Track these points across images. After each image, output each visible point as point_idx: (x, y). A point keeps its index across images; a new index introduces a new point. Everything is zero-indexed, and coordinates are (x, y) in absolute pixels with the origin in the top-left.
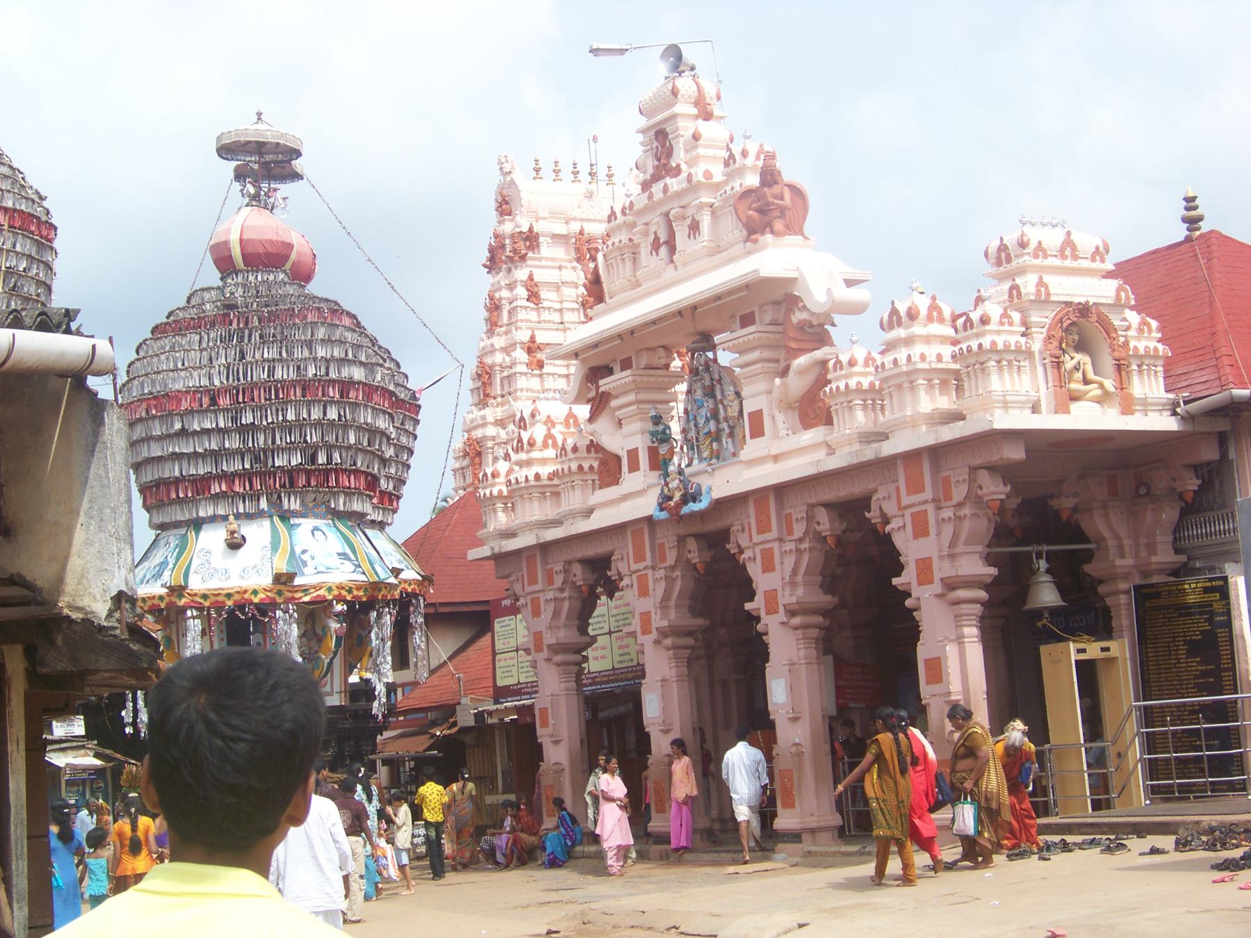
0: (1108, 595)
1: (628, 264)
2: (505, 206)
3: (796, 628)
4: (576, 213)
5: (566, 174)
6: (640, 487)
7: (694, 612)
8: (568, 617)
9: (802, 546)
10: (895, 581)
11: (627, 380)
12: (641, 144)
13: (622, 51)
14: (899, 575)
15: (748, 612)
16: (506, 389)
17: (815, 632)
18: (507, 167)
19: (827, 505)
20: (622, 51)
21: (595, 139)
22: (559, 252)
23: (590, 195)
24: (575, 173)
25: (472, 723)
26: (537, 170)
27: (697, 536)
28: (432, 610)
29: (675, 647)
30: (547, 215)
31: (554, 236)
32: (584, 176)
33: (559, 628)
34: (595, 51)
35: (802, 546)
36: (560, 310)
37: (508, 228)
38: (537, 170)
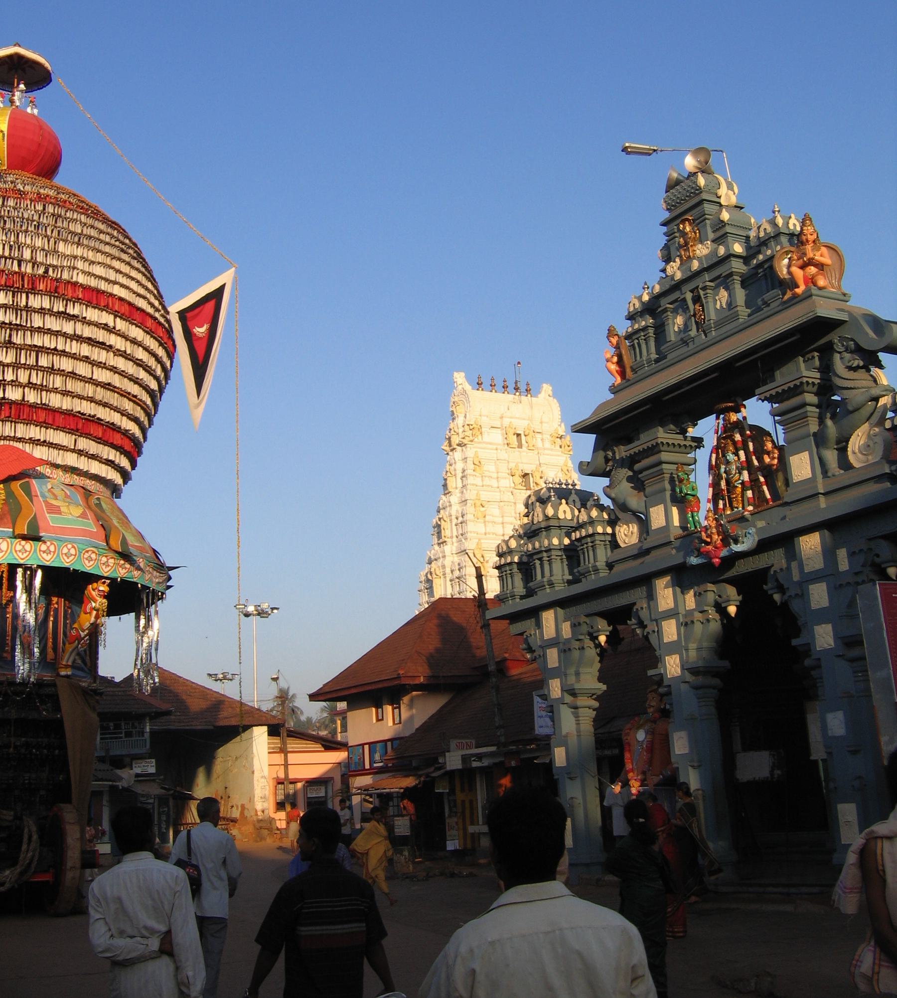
15: (794, 647)
19: (885, 537)
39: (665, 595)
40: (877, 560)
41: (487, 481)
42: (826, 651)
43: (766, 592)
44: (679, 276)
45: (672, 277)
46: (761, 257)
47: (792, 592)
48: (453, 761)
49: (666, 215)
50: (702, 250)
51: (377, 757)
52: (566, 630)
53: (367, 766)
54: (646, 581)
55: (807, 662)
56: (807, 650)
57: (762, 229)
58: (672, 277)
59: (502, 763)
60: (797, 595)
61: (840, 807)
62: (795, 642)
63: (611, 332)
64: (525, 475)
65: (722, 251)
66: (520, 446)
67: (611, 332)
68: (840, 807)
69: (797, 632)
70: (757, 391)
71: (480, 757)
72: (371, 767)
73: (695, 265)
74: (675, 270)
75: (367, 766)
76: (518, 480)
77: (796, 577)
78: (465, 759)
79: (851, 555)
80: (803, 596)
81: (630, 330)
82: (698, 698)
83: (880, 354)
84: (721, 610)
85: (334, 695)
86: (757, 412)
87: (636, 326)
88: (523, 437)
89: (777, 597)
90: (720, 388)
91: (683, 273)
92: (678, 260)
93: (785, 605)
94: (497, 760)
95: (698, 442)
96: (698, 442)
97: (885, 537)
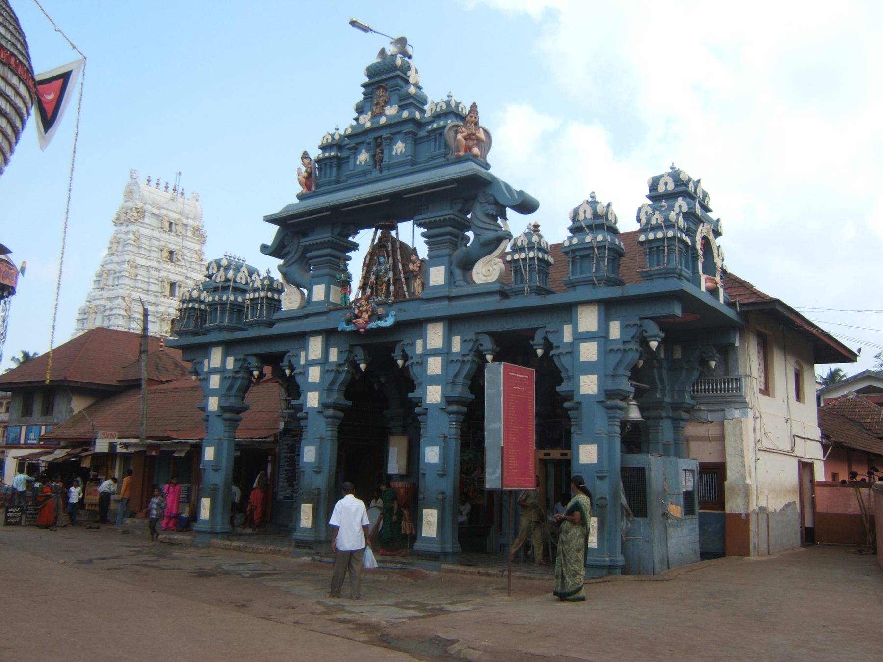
0: (420, 415)
1: (334, 170)
2: (130, 193)
3: (450, 413)
4: (165, 206)
5: (162, 187)
6: (325, 310)
7: (347, 396)
8: (465, 377)
9: (466, 359)
10: (410, 395)
11: (326, 240)
12: (363, 93)
13: (366, 29)
14: (413, 392)
15: (410, 399)
16: (116, 283)
17: (461, 418)
18: (134, 176)
19: (489, 334)
20: (366, 29)
21: (180, 174)
22: (154, 222)
23: (173, 199)
24: (167, 188)
25: (106, 450)
26: (149, 181)
27: (363, 346)
28: (745, 309)
29: (333, 417)
30: (151, 202)
31: (153, 214)
32: (170, 190)
33: (230, 396)
34: (353, 23)
35: (341, 369)
36: (150, 250)
37: (130, 204)
38: (149, 181)
39: (315, 347)
40: (481, 348)
41: (142, 251)
42: (590, 396)
43: (532, 346)
44: (368, 125)
45: (364, 124)
46: (435, 125)
47: (415, 360)
48: (101, 446)
49: (366, 80)
50: (391, 111)
51: (32, 436)
52: (230, 363)
53: (22, 441)
54: (302, 337)
55: (417, 410)
56: (419, 402)
57: (439, 106)
58: (364, 124)
59: (145, 452)
60: (418, 363)
61: (425, 511)
62: (410, 395)
63: (305, 156)
64: (171, 252)
65: (405, 114)
66: (170, 231)
67: (305, 156)
68: (425, 511)
69: (412, 388)
70: (416, 218)
71: (126, 446)
72: (25, 443)
73: (383, 120)
74: (366, 121)
75: (22, 441)
76: (166, 254)
77: (205, 369)
78: (112, 446)
79: (464, 341)
80: (305, 374)
81: (321, 156)
82: (745, 402)
83: (508, 209)
84: (644, 342)
85: (6, 387)
86: (409, 233)
87: (327, 155)
88: (173, 226)
89: (287, 372)
90: (385, 212)
91: (372, 123)
92: (370, 113)
93: (405, 369)
94: (138, 449)
95: (355, 247)
96: (355, 247)
97: (489, 334)
